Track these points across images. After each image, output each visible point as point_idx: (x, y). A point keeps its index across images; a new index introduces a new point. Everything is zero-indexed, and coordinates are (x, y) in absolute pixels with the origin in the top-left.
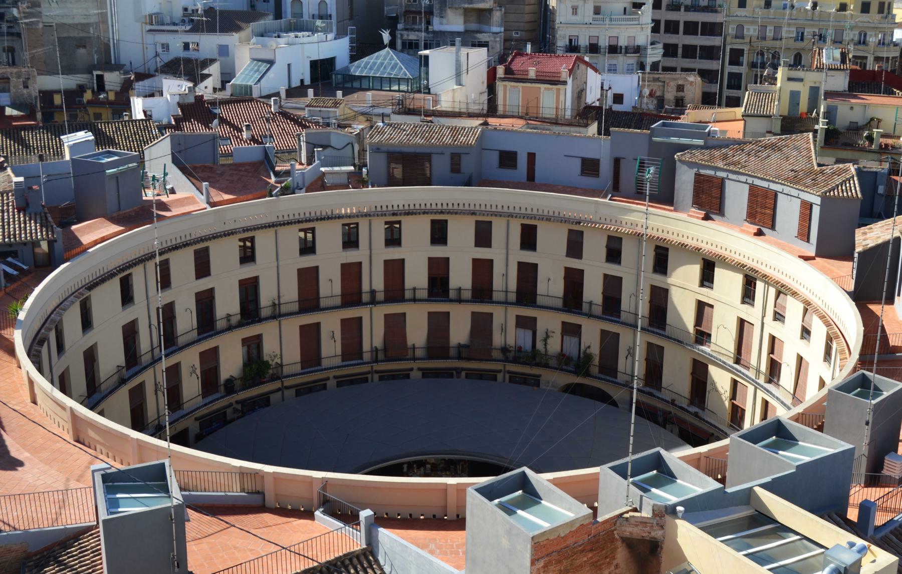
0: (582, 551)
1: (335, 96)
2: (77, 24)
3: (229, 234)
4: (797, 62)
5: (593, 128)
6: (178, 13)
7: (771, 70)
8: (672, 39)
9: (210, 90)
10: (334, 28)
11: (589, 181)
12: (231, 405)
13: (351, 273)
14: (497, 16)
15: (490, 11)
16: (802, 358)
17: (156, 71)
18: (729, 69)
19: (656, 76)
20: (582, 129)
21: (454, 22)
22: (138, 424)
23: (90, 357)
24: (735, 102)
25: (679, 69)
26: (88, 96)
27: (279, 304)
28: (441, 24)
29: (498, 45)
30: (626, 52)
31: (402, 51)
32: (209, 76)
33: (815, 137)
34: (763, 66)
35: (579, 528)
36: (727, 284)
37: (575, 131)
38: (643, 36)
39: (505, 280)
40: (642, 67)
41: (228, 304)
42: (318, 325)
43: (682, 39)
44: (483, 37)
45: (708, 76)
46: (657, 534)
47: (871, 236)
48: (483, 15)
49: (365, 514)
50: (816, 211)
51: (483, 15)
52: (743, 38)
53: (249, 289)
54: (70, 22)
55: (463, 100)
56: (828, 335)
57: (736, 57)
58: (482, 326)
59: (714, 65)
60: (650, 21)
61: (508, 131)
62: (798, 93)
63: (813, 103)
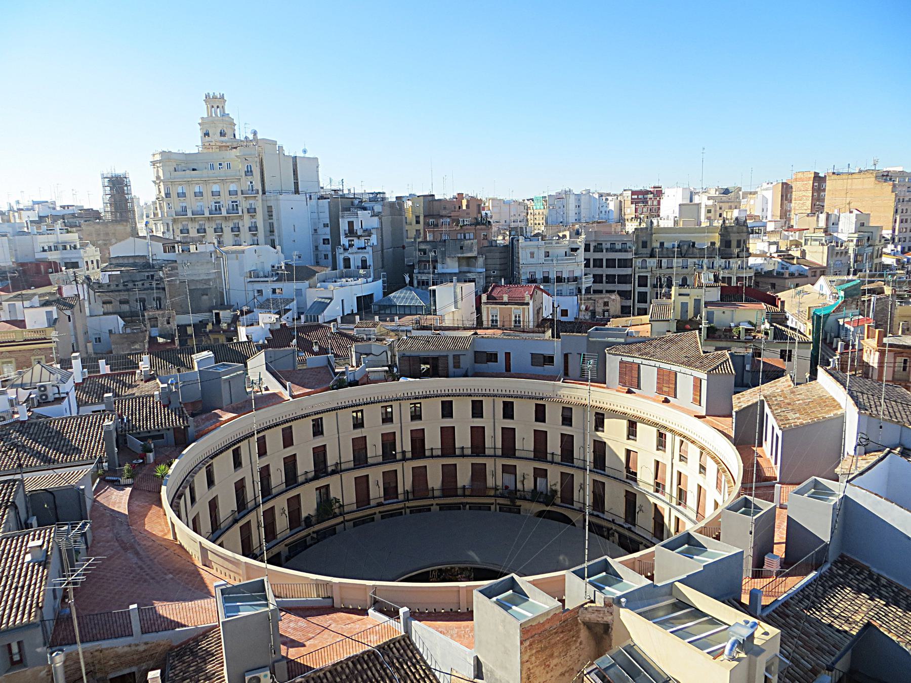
8: (598, 271)
12: (309, 534)
14: (481, 260)
18: (638, 289)
20: (541, 335)
21: (451, 266)
22: (247, 551)
24: (644, 312)
26: (210, 327)
32: (289, 310)
33: (700, 333)
34: (661, 287)
35: (552, 617)
39: (493, 441)
40: (580, 291)
41: (305, 465)
43: (605, 271)
45: (624, 295)
46: (608, 619)
49: (403, 610)
52: (646, 268)
53: (320, 454)
57: (643, 282)
58: (479, 472)
63: (697, 311)
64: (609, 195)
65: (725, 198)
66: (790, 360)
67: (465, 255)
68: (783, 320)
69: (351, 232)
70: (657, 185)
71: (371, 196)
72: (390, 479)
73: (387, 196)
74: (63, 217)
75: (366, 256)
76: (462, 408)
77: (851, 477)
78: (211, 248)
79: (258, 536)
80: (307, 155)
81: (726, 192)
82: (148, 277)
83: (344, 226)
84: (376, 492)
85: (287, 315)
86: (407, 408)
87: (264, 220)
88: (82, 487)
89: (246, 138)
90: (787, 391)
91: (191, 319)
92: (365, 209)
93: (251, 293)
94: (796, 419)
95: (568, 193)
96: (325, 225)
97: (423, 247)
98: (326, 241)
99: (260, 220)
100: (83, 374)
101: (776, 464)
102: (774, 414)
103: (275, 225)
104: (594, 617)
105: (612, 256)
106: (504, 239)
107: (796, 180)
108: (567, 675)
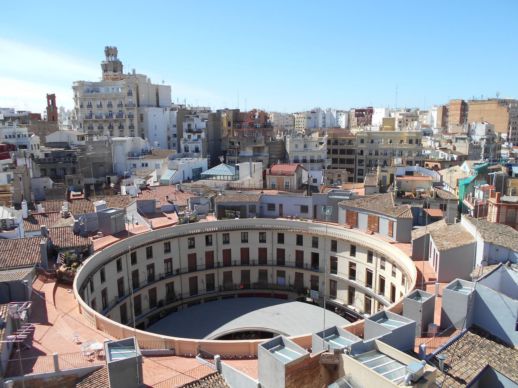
8: (335, 156)
9: (152, 182)
12: (161, 311)
13: (210, 255)
14: (266, 149)
15: (263, 147)
18: (358, 167)
23: (104, 293)
24: (361, 181)
26: (104, 186)
32: (152, 177)
35: (306, 359)
36: (361, 258)
38: (324, 156)
40: (324, 168)
41: (160, 269)
43: (339, 156)
44: (260, 158)
46: (336, 361)
47: (419, 232)
49: (217, 357)
50: (395, 224)
58: (263, 274)
59: (352, 166)
64: (342, 111)
67: (257, 146)
70: (370, 106)
73: (212, 109)
74: (19, 118)
75: (199, 145)
77: (478, 279)
78: (105, 138)
79: (131, 312)
80: (165, 84)
82: (68, 155)
83: (185, 126)
84: (202, 286)
88: (25, 281)
89: (129, 73)
93: (129, 166)
94: (448, 245)
96: (174, 126)
97: (233, 140)
98: (175, 136)
100: (28, 212)
101: (436, 271)
102: (435, 242)
104: (329, 361)
106: (280, 136)
107: (451, 104)
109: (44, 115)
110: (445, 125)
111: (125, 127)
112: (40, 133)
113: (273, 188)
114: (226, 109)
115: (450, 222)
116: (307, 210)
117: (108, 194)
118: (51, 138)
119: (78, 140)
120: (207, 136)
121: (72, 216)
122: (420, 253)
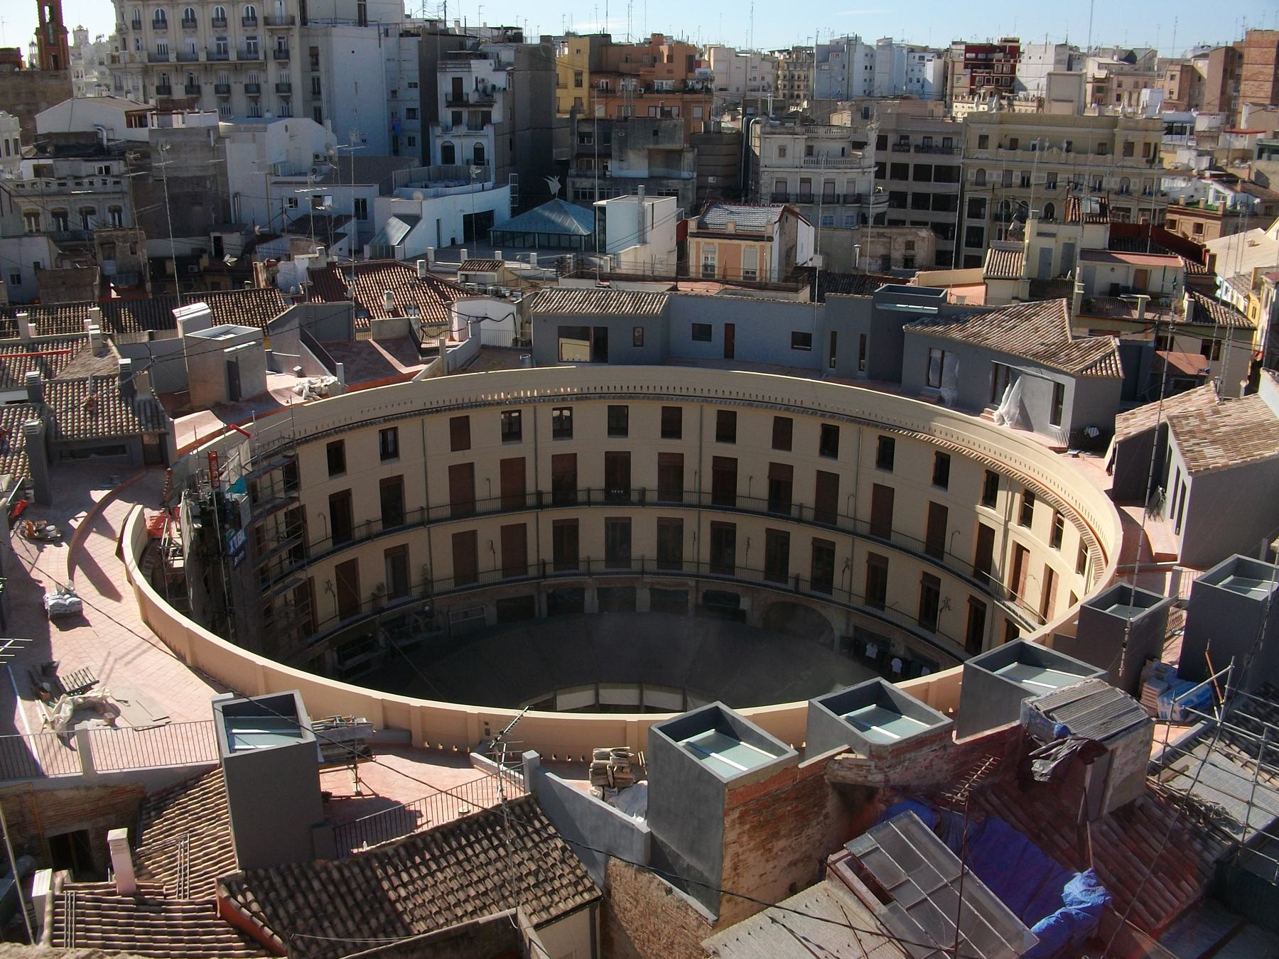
0: (786, 799)
1: (494, 255)
2: (191, 178)
3: (367, 425)
4: (1049, 214)
5: (804, 295)
6: (308, 161)
7: (1019, 224)
8: (899, 186)
10: (493, 176)
11: (801, 355)
13: (513, 470)
14: (689, 157)
15: (680, 153)
16: (1051, 571)
17: (283, 230)
18: (968, 222)
19: (881, 231)
20: (791, 295)
21: (636, 165)
24: (976, 262)
25: (908, 222)
26: (205, 261)
27: (428, 508)
28: (621, 169)
29: (690, 194)
30: (845, 202)
31: (574, 203)
32: (344, 235)
33: (1069, 305)
34: (1008, 219)
37: (782, 297)
38: (865, 182)
40: (863, 220)
41: (366, 508)
42: (474, 533)
44: (674, 184)
45: (942, 230)
47: (1134, 422)
48: (672, 157)
51: (672, 157)
52: (984, 184)
53: (392, 491)
54: (185, 174)
55: (648, 260)
56: (1082, 540)
57: (976, 208)
59: (952, 218)
60: (873, 163)
61: (702, 296)
62: (1050, 250)
63: (1068, 264)
64: (925, 49)
65: (1127, 67)
66: (1216, 358)
67: (661, 147)
68: (1210, 288)
69: (458, 97)
70: (1011, 36)
71: (496, 33)
72: (514, 538)
75: (484, 142)
76: (645, 419)
81: (1130, 57)
83: (445, 85)
84: (489, 559)
85: (339, 245)
86: (547, 415)
87: (303, 72)
90: (1207, 410)
91: (173, 246)
92: (484, 56)
93: (277, 204)
94: (1215, 457)
95: (852, 42)
98: (411, 112)
99: (295, 73)
103: (323, 81)
104: (851, 776)
105: (924, 159)
108: (800, 865)
109: (28, 55)
110: (1229, 105)
111: (264, 87)
112: (20, 108)
113: (708, 275)
114: (568, 34)
115: (1227, 393)
116: (555, 528)
117: (216, 286)
118: (50, 121)
119: (130, 125)
120: (512, 112)
121: (114, 349)
122: (1137, 480)
